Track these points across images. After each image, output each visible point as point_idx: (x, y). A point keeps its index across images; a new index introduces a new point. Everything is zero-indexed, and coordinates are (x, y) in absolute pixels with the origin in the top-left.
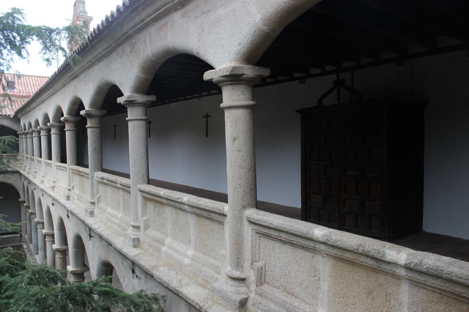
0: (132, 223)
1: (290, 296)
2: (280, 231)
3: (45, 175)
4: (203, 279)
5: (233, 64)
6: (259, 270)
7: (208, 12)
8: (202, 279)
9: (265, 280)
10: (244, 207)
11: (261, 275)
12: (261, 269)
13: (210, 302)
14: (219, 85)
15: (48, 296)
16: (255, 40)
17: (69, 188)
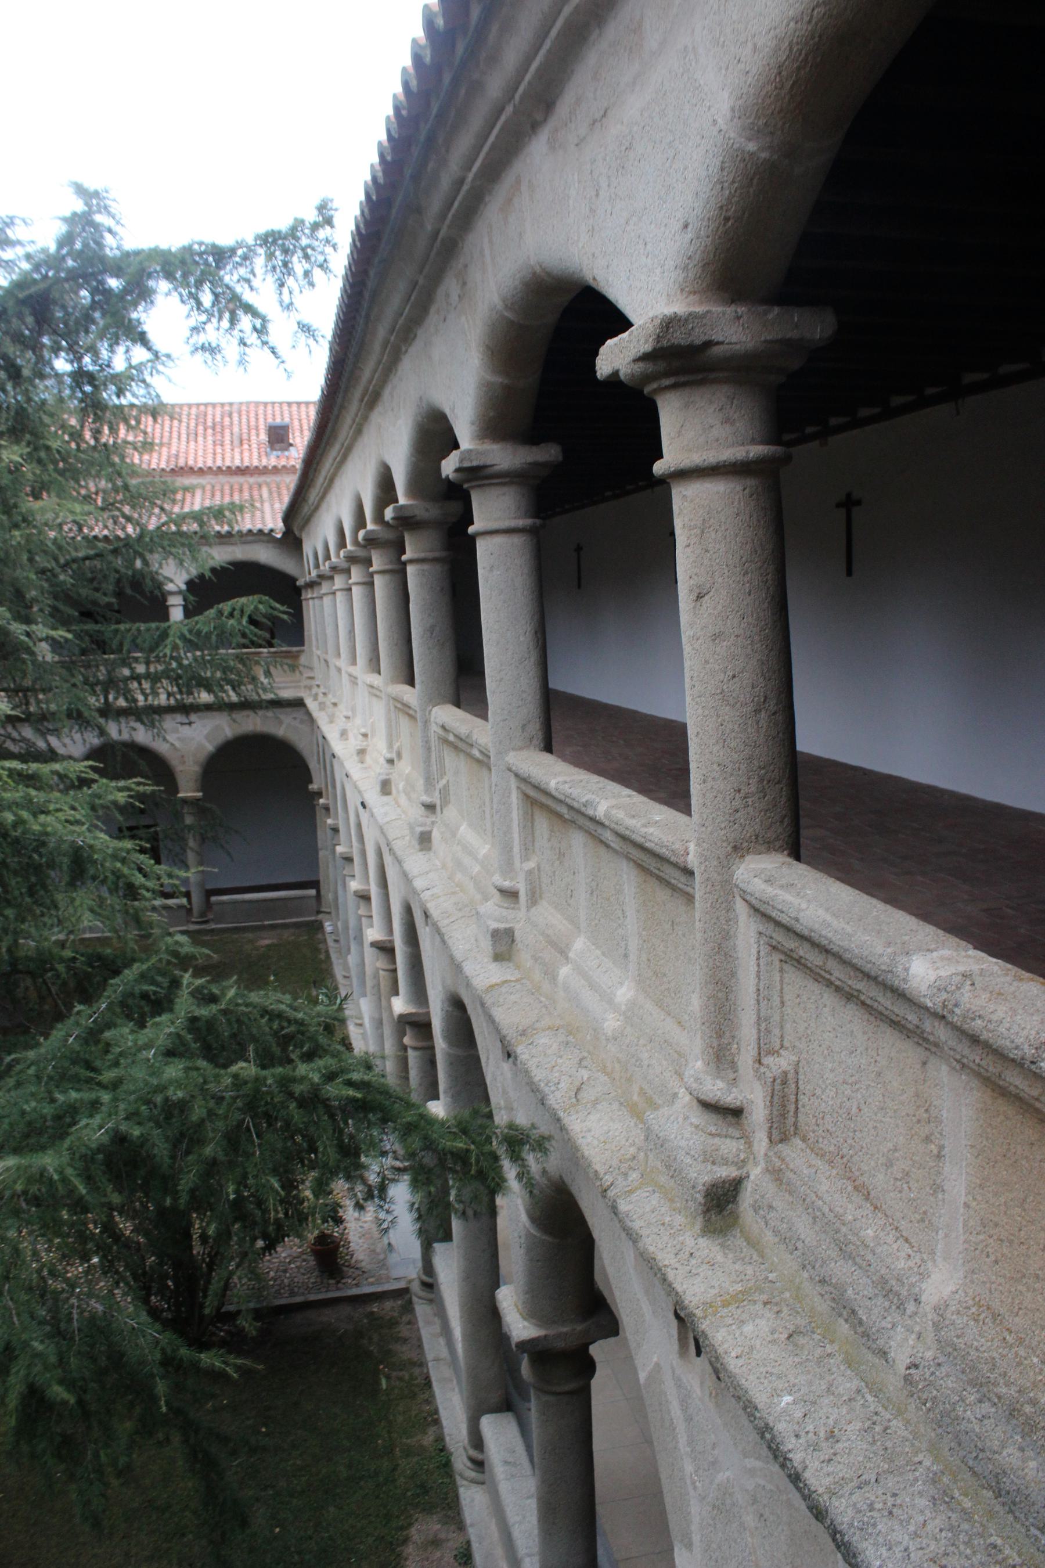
0: (498, 880)
1: (858, 1199)
2: (825, 951)
3: (350, 714)
4: (642, 1092)
5: (678, 307)
6: (777, 1087)
7: (605, 115)
8: (641, 1089)
9: (795, 1125)
10: (739, 850)
11: (784, 1106)
12: (784, 1083)
13: (634, 1175)
14: (647, 390)
15: (193, 1096)
16: (729, 199)
17: (389, 756)
